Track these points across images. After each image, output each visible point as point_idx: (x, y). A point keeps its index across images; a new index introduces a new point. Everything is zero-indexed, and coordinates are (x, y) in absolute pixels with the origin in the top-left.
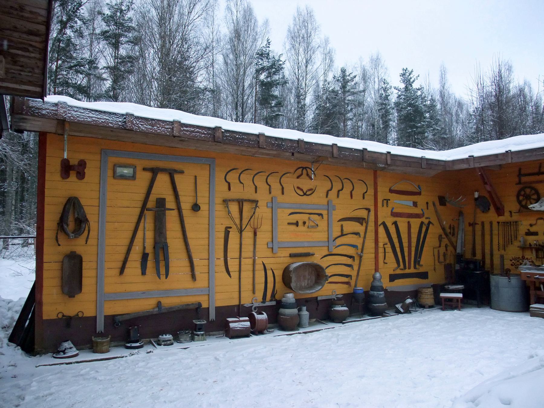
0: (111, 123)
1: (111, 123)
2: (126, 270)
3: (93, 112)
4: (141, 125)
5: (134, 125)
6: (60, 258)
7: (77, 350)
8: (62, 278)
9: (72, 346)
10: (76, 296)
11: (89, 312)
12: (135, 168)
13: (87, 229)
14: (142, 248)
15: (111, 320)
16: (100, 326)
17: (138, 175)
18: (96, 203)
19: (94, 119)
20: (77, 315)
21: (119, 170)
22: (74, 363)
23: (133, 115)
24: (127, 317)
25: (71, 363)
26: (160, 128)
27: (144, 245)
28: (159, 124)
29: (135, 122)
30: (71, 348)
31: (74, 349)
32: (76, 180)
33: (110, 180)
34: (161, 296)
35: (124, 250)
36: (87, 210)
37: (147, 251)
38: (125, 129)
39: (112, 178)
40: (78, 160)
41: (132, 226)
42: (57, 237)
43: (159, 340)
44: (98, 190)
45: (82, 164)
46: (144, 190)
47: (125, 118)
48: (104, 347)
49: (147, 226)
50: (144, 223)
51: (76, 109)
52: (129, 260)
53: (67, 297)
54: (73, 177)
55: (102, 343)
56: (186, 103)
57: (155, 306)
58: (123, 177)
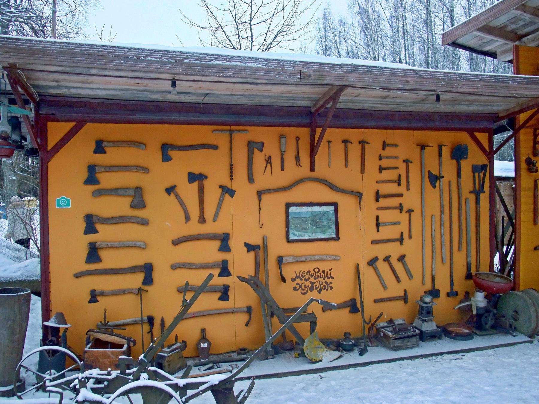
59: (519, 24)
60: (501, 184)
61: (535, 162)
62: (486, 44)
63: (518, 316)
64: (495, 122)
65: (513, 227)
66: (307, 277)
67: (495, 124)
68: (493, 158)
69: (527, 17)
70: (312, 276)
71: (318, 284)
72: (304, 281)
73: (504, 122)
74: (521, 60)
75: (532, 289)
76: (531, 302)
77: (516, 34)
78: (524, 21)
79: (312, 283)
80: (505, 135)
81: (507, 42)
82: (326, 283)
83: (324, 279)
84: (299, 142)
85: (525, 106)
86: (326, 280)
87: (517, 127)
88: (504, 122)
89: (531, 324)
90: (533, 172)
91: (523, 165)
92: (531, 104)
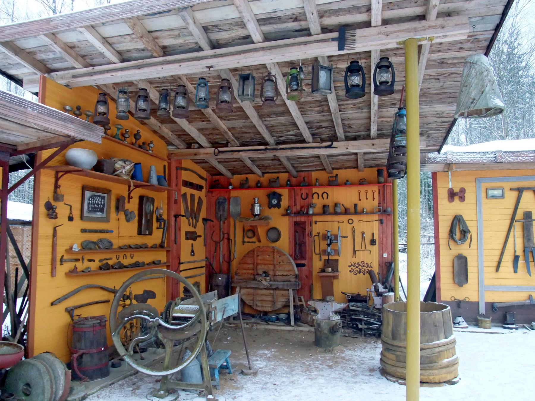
0: (485, 160)
1: (485, 160)
2: (501, 268)
3: (471, 154)
4: (509, 157)
5: (503, 158)
6: (451, 258)
7: (468, 324)
8: (453, 272)
9: (464, 320)
10: (464, 286)
11: (473, 298)
12: (503, 189)
13: (469, 237)
14: (513, 251)
15: (492, 307)
16: (482, 309)
17: (506, 195)
18: (474, 218)
19: (472, 159)
20: (465, 299)
21: (491, 193)
22: (467, 332)
23: (501, 151)
24: (503, 305)
25: (465, 332)
26: (525, 157)
27: (515, 249)
28: (524, 154)
29: (503, 156)
30: (463, 322)
31: (465, 323)
32: (459, 202)
33: (484, 201)
34: (531, 290)
35: (498, 253)
36: (468, 223)
37: (517, 254)
38: (496, 162)
39: (486, 199)
40: (459, 188)
41: (504, 234)
42: (449, 244)
43: (532, 326)
44: (476, 208)
45: (463, 191)
46: (512, 206)
47: (495, 154)
48: (487, 325)
49: (516, 234)
50: (514, 231)
51: (459, 154)
52: (502, 260)
53: (457, 286)
54: (456, 199)
55: (486, 321)
56: (504, 79)
57: (527, 298)
58: (494, 197)
59: (48, 55)
60: (25, 229)
61: (55, 207)
62: (12, 66)
63: (30, 389)
64: (11, 155)
65: (28, 280)
66: (357, 266)
67: (11, 158)
68: (7, 197)
69: (57, 49)
70: (360, 265)
71: (363, 270)
72: (355, 268)
73: (24, 158)
74: (47, 94)
75: (47, 352)
76: (45, 370)
77: (45, 65)
78: (54, 54)
79: (360, 269)
80: (22, 173)
81: (35, 71)
82: (368, 270)
83: (367, 267)
84: (361, 194)
85: (46, 144)
86: (368, 268)
87: (38, 163)
88: (24, 158)
89: (44, 397)
90: (51, 218)
91: (42, 210)
92: (52, 142)
